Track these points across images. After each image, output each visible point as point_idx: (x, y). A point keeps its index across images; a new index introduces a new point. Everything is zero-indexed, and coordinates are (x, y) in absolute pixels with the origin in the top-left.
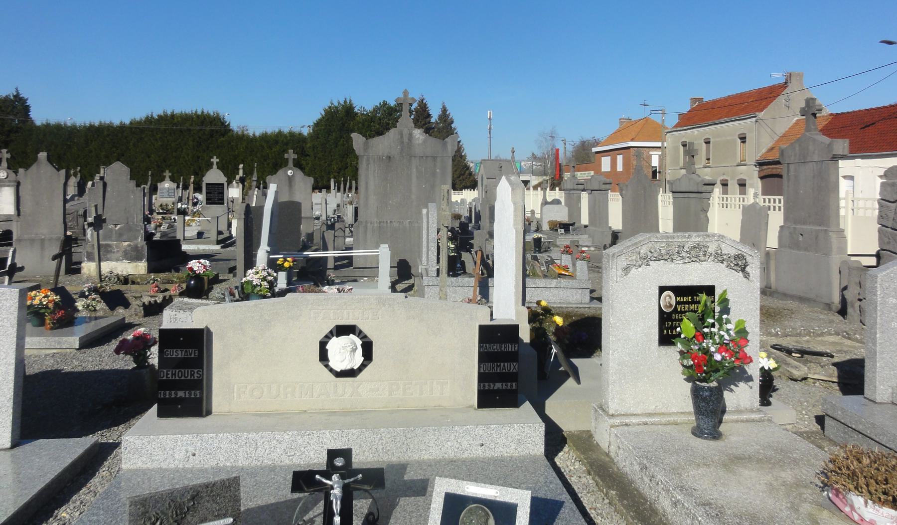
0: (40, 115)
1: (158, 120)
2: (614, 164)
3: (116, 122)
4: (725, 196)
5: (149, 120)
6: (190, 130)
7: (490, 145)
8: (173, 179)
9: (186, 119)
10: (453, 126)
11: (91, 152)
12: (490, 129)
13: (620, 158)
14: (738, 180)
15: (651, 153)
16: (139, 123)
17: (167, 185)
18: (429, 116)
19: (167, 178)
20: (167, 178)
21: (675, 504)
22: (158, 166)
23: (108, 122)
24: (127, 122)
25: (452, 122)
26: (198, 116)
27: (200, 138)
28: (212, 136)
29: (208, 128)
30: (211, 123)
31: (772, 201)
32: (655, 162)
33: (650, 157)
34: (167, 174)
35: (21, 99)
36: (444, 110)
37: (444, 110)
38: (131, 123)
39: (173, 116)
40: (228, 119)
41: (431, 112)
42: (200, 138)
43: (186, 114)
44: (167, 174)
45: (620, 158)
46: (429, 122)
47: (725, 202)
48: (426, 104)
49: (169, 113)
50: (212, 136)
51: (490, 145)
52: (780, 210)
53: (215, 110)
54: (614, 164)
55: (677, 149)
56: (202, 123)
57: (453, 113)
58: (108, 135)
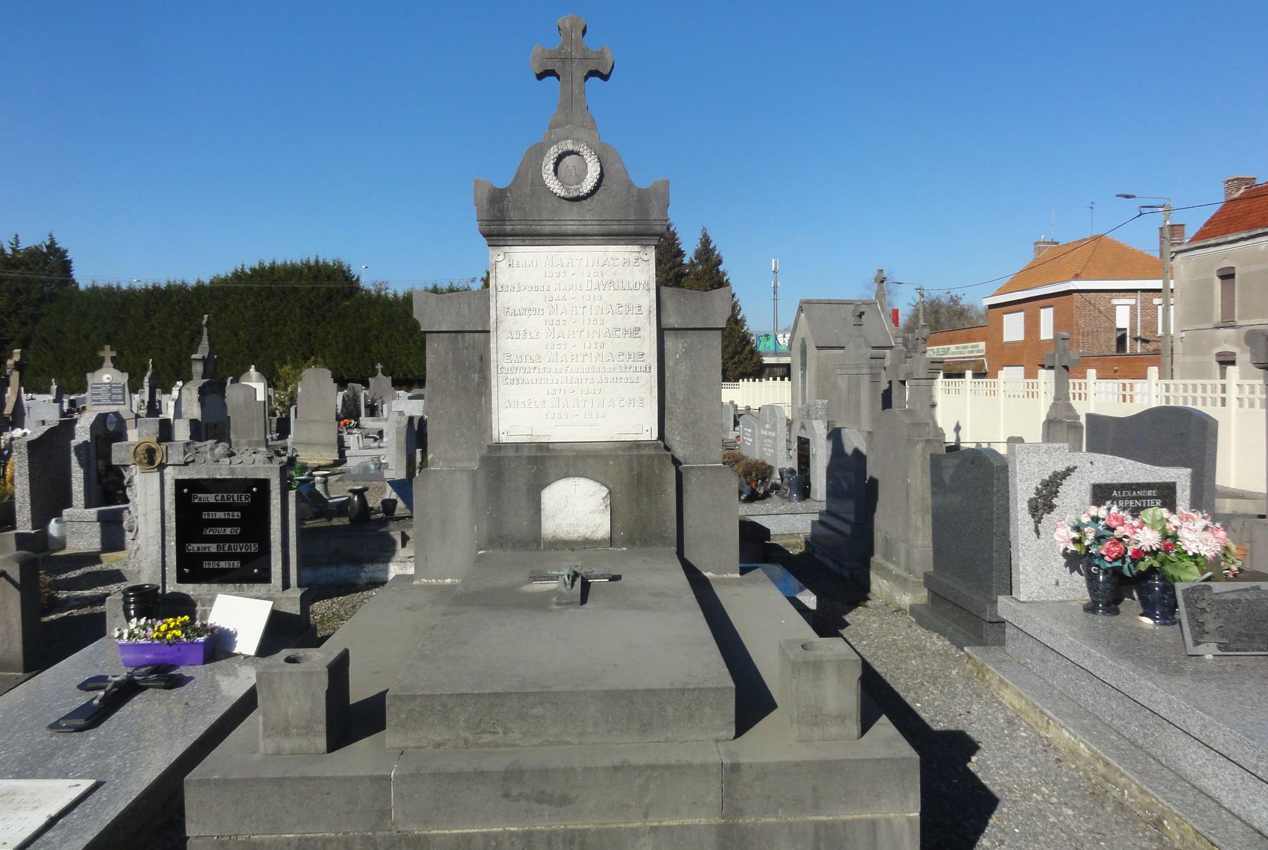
0: (85, 275)
1: (251, 276)
2: (1032, 325)
3: (191, 282)
4: (1030, 381)
5: (239, 276)
6: (295, 290)
7: (776, 312)
8: (118, 364)
9: (292, 272)
10: (721, 268)
11: (153, 328)
12: (775, 287)
13: (1047, 317)
14: (1219, 355)
15: (1115, 302)
16: (225, 280)
17: (107, 376)
18: (680, 253)
19: (108, 363)
20: (108, 363)
21: (921, 649)
22: (250, 350)
23: (179, 282)
24: (207, 281)
25: (720, 262)
26: (310, 268)
27: (311, 302)
28: (330, 299)
29: (325, 285)
30: (329, 278)
31: (1199, 388)
32: (1123, 319)
33: (1110, 313)
34: (108, 353)
35: (58, 250)
36: (706, 241)
37: (706, 241)
38: (212, 282)
39: (273, 268)
40: (355, 271)
41: (682, 247)
42: (311, 302)
43: (293, 265)
44: (108, 353)
45: (1047, 317)
46: (681, 264)
47: (1030, 390)
48: (674, 234)
49: (267, 264)
50: (330, 299)
51: (776, 312)
52: (1252, 405)
53: (335, 257)
54: (1032, 325)
55: (1209, 285)
56: (316, 278)
57: (721, 246)
58: (179, 302)
